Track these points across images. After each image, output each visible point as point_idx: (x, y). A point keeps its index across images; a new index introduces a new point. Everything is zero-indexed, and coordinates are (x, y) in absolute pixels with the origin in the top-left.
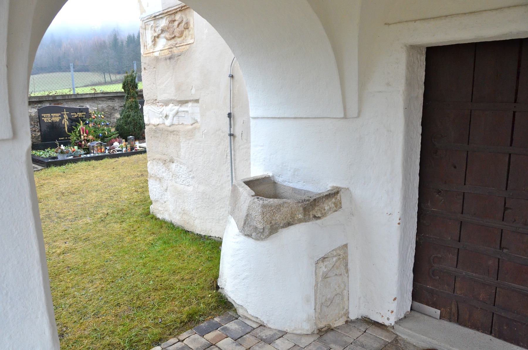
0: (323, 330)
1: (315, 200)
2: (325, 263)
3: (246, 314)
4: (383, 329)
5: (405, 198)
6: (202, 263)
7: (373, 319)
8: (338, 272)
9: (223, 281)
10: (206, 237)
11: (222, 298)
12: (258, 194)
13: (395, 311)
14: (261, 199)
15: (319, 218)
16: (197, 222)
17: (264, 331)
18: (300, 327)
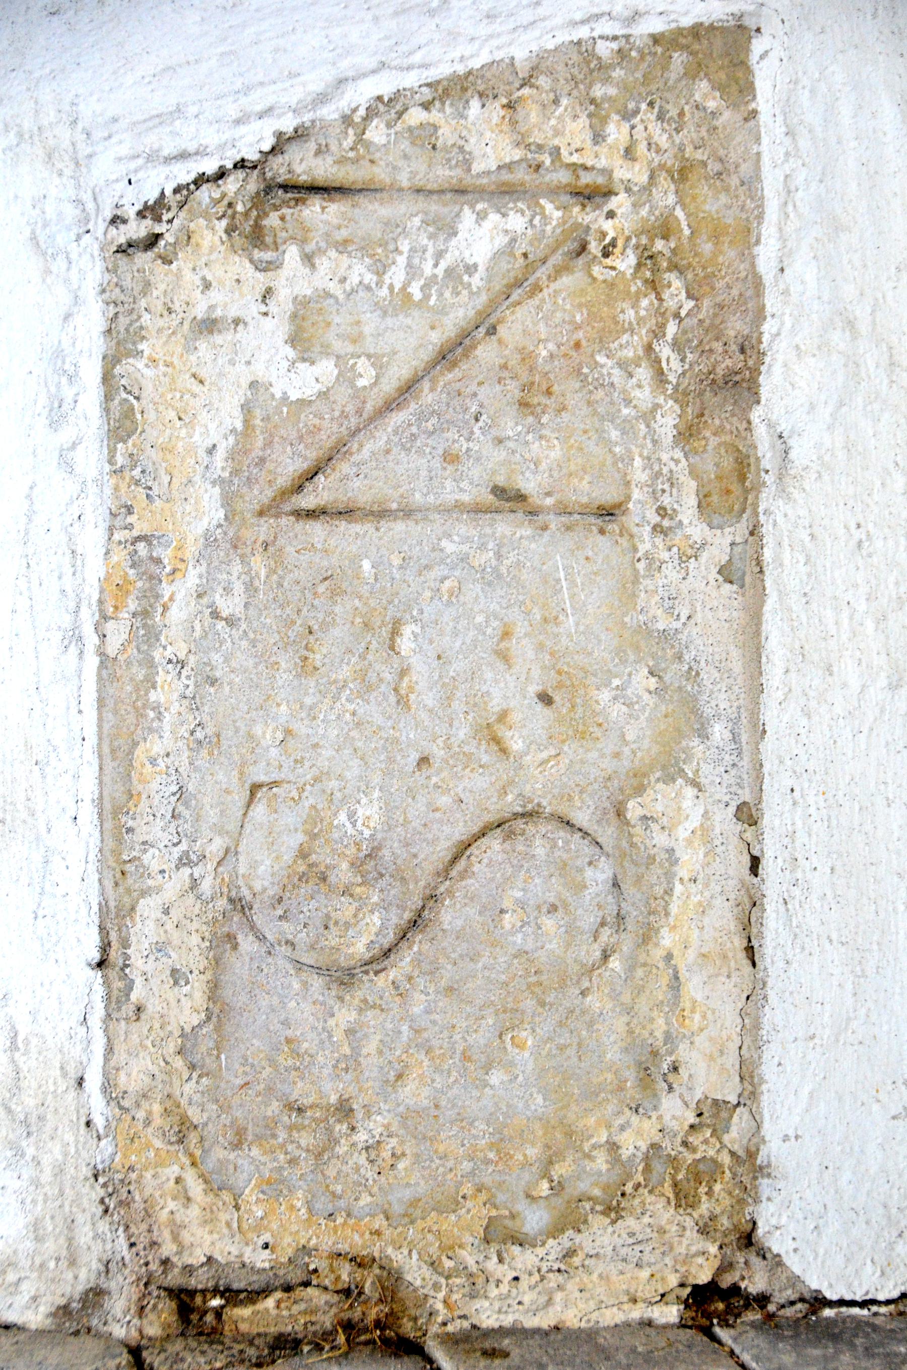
2: (293, 278)
8: (541, 461)
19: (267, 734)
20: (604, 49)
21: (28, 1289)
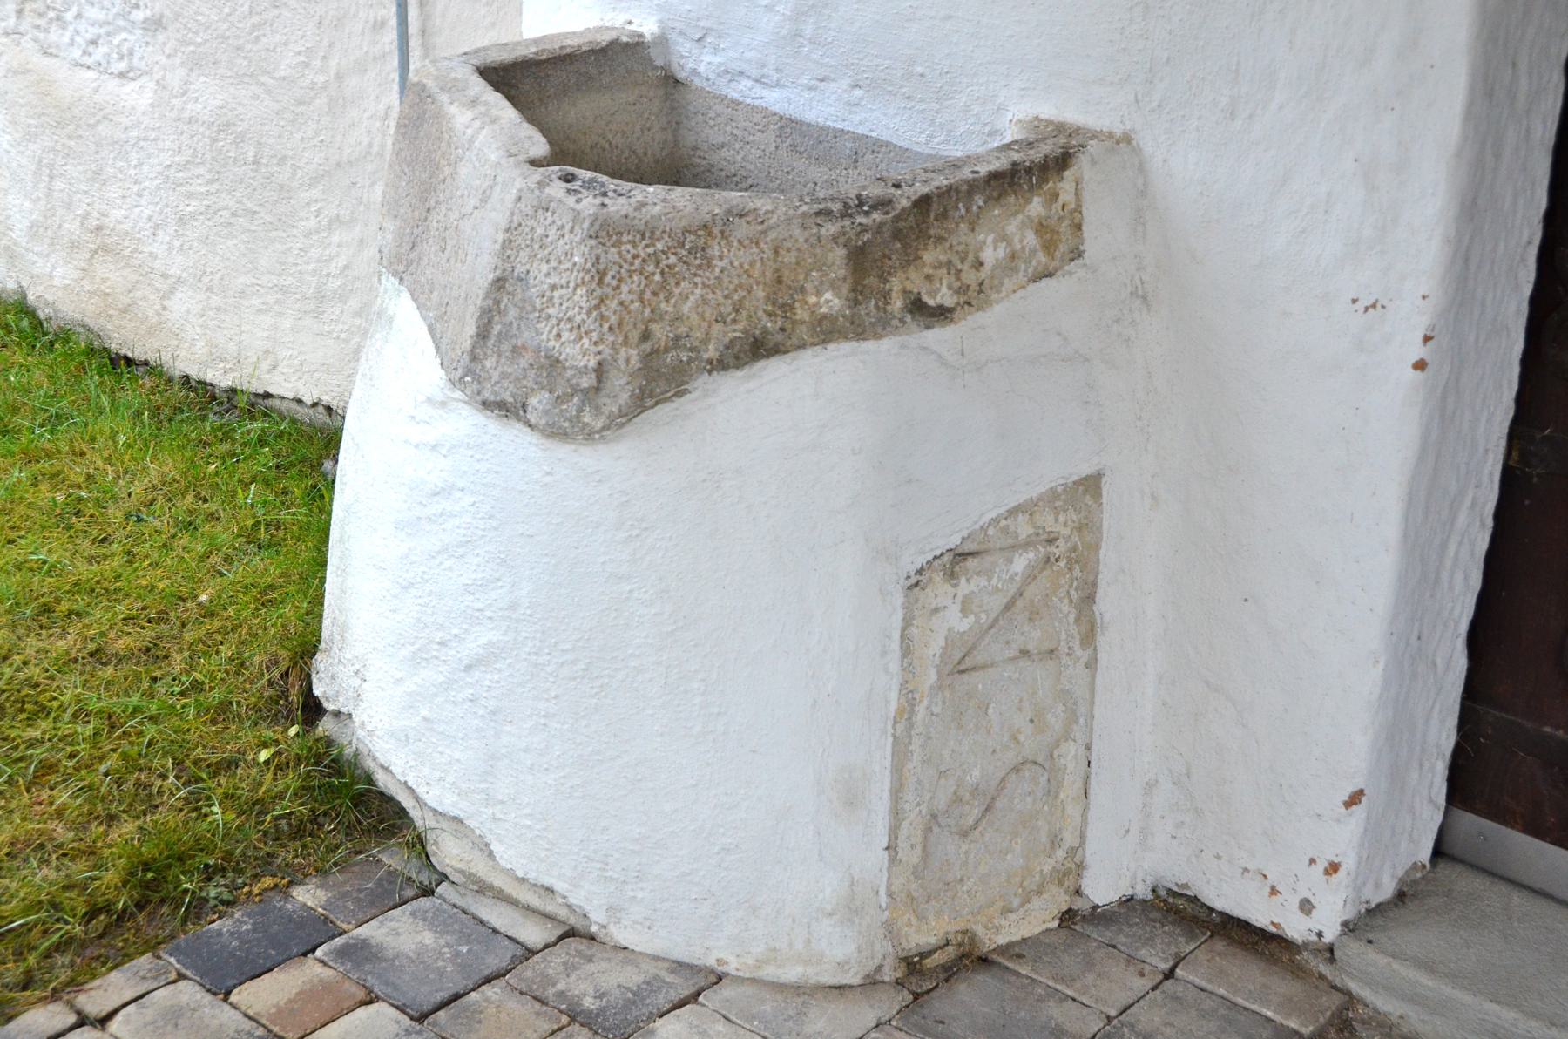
0: (929, 963)
1: (923, 202)
2: (964, 587)
3: (480, 868)
4: (1272, 960)
5: (1473, 209)
6: (216, 559)
7: (1219, 905)
8: (1034, 637)
9: (345, 673)
10: (242, 402)
11: (339, 773)
12: (566, 154)
13: (1349, 864)
14: (589, 185)
15: (941, 314)
16: (183, 304)
17: (591, 968)
18: (799, 946)
19: (946, 753)
20: (1060, 489)
21: (853, 970)
